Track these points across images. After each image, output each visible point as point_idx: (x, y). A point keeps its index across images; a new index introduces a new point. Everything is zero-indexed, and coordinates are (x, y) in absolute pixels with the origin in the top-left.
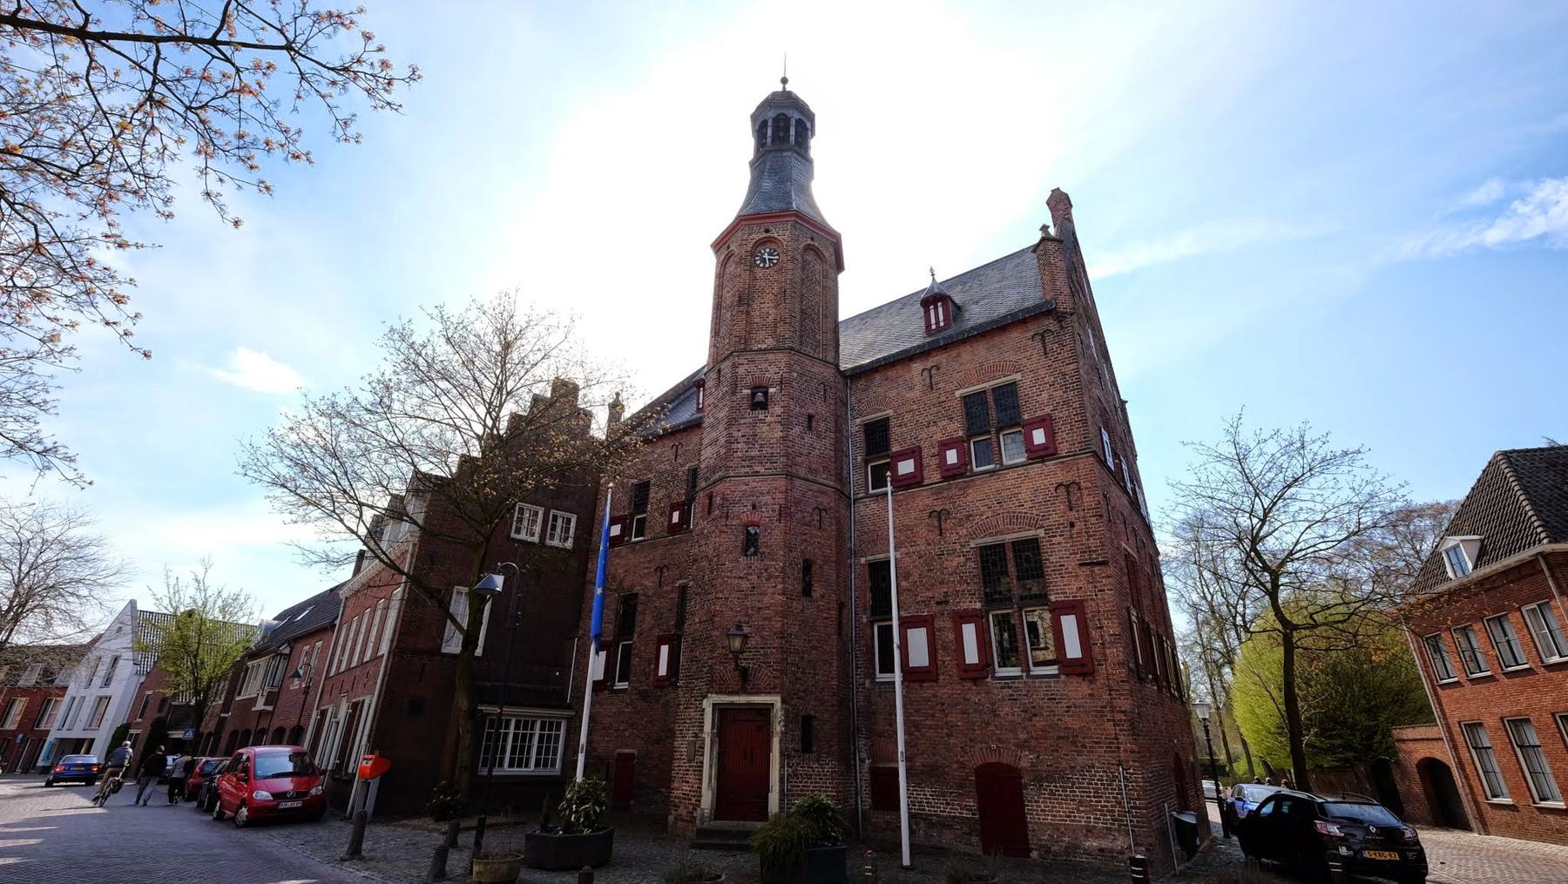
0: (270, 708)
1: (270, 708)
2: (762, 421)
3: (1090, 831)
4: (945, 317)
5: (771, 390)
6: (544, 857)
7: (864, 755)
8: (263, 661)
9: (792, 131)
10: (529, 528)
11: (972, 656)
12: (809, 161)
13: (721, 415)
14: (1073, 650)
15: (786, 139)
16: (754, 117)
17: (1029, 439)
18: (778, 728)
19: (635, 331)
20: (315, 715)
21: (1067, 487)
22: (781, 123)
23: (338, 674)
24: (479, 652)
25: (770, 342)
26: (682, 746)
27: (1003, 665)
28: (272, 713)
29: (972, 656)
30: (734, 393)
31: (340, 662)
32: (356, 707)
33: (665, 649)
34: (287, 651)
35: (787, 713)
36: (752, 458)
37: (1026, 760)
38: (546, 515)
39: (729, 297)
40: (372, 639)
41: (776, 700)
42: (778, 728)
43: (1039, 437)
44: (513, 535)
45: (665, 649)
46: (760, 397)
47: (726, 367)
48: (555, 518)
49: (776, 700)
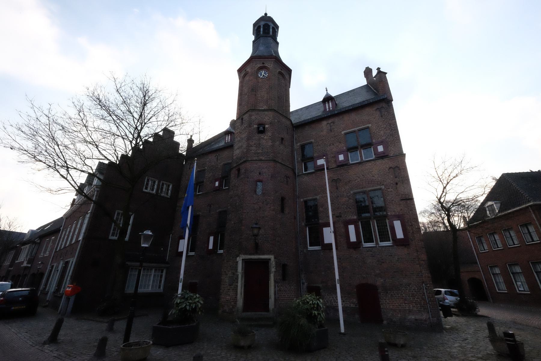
0: (29, 265)
1: (29, 265)
2: (263, 138)
3: (410, 311)
4: (332, 108)
5: (267, 126)
6: (165, 338)
7: (304, 281)
8: (28, 246)
9: (271, 30)
10: (151, 187)
11: (353, 238)
12: (278, 43)
13: (243, 136)
14: (400, 234)
15: (269, 33)
16: (255, 25)
17: (376, 150)
18: (273, 270)
19: (203, 108)
20: (49, 267)
21: (394, 168)
22: (266, 27)
23: (60, 250)
24: (127, 239)
25: (265, 107)
26: (226, 279)
27: (245, 261)
28: (30, 267)
29: (353, 238)
30: (250, 126)
31: (62, 244)
32: (67, 263)
33: (212, 239)
34: (39, 241)
35: (276, 263)
36: (258, 153)
37: (379, 282)
38: (159, 182)
39: (246, 90)
40: (76, 233)
41: (272, 257)
42: (273, 270)
43: (380, 149)
44: (144, 190)
45: (212, 239)
46: (261, 128)
47: (246, 117)
48: (163, 184)
49: (272, 257)
